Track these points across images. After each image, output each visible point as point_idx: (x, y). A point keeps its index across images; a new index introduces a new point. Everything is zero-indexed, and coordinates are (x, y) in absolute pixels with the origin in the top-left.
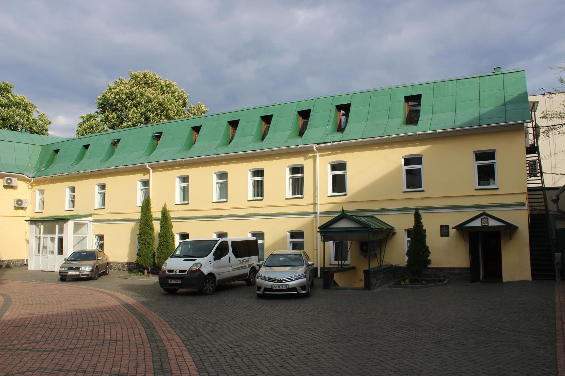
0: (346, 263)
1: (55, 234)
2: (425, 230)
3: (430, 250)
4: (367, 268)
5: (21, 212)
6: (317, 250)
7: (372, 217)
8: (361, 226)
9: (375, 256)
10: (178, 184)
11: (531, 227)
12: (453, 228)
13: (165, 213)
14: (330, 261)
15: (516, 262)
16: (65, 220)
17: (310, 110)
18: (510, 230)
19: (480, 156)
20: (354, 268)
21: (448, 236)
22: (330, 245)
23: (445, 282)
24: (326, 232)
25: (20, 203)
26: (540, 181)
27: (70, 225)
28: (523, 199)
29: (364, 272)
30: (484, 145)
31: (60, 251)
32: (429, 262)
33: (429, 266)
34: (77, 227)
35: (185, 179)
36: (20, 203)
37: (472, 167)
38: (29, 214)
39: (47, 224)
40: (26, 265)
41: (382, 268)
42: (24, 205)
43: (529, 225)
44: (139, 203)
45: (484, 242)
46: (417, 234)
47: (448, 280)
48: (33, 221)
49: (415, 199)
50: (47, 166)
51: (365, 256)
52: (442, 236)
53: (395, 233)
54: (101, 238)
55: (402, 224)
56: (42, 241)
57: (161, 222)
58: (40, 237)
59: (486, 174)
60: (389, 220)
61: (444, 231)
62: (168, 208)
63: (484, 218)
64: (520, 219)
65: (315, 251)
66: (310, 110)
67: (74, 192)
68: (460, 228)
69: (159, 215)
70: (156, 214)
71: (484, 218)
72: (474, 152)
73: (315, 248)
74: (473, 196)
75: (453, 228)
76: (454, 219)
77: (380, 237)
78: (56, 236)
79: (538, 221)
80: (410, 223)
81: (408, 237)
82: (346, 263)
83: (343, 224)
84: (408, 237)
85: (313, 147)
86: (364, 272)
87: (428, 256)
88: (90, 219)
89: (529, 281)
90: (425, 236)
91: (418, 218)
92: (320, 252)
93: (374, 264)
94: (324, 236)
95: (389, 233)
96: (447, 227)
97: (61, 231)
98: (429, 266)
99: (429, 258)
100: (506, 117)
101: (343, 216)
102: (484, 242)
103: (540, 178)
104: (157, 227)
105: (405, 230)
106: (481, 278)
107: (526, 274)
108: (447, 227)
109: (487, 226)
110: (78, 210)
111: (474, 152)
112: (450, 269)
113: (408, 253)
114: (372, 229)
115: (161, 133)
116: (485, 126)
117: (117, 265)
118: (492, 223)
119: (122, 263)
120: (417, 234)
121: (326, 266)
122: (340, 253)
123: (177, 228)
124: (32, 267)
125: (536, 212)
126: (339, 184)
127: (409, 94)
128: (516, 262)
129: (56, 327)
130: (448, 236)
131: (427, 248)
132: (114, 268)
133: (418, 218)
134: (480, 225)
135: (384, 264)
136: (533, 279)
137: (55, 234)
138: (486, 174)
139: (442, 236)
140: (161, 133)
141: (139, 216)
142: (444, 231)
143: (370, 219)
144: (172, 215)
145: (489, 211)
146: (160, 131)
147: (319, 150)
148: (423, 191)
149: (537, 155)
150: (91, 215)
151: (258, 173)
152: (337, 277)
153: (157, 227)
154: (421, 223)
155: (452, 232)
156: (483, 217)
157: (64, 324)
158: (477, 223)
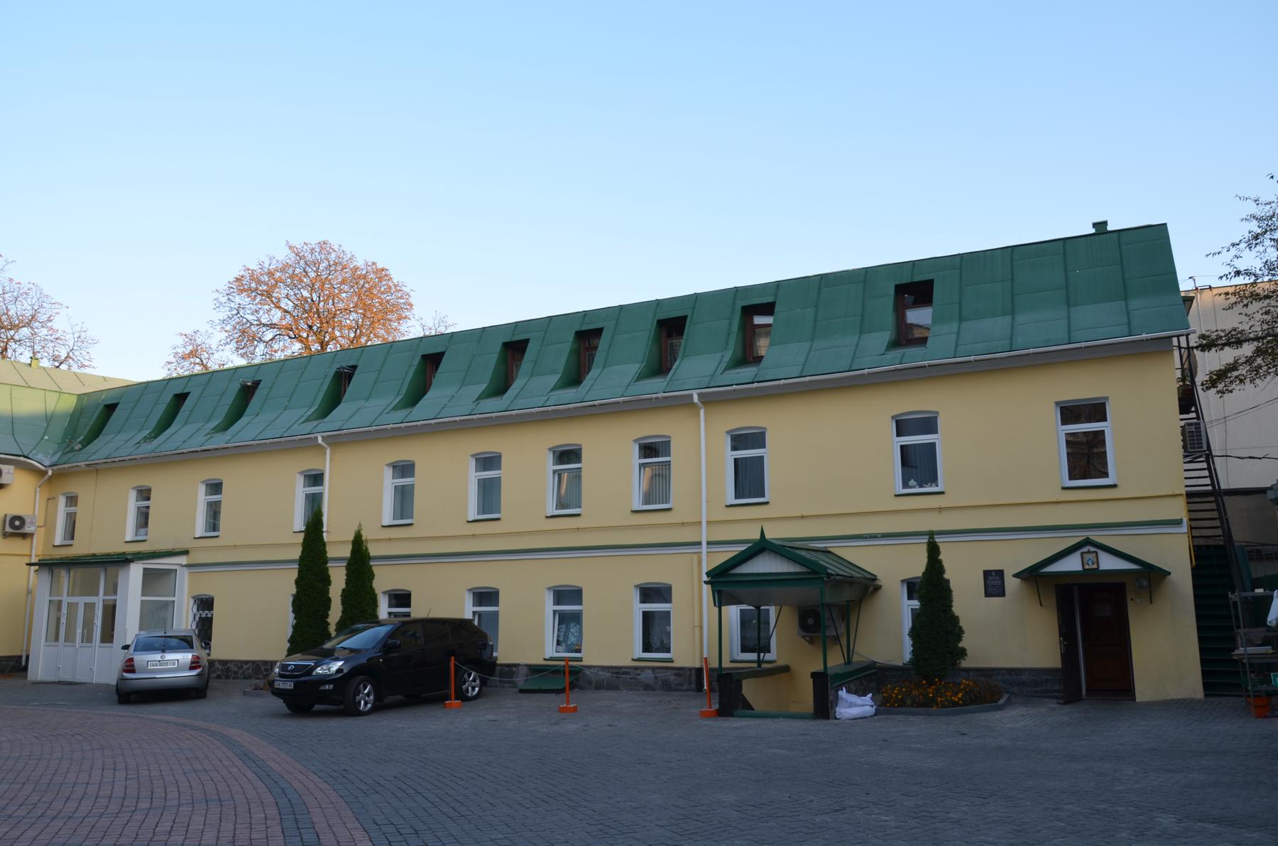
0: (768, 657)
1: (97, 594)
2: (948, 581)
3: (962, 624)
4: (819, 667)
5: (17, 546)
6: (701, 627)
7: (826, 552)
8: (804, 570)
9: (837, 639)
10: (389, 482)
11: (1197, 573)
12: (1016, 576)
13: (358, 543)
14: (731, 652)
15: (1165, 650)
16: (124, 560)
17: (685, 318)
18: (1150, 577)
19: (1070, 413)
20: (786, 669)
21: (1003, 594)
22: (733, 613)
23: (1001, 702)
24: (724, 582)
25: (17, 523)
26: (1206, 473)
27: (136, 572)
28: (1178, 510)
29: (814, 675)
30: (1080, 385)
31: (108, 636)
32: (963, 653)
33: (965, 664)
34: (151, 577)
35: (404, 469)
36: (17, 523)
37: (1053, 439)
38: (38, 549)
39: (78, 572)
40: (25, 669)
41: (850, 668)
42: (27, 529)
43: (1193, 569)
44: (299, 523)
45: (1093, 607)
46: (931, 589)
47: (1006, 696)
48: (48, 565)
49: (923, 514)
50: (87, 442)
51: (811, 642)
52: (987, 594)
53: (878, 588)
54: (205, 603)
55: (896, 566)
56: (64, 610)
57: (348, 568)
58: (60, 602)
59: (1087, 458)
60: (864, 558)
61: (993, 583)
62: (366, 535)
63: (1089, 552)
64: (1174, 554)
65: (697, 630)
66: (685, 318)
67: (148, 499)
68: (1033, 576)
69: (346, 552)
70: (338, 548)
71: (1089, 552)
72: (1057, 403)
73: (697, 623)
74: (1057, 503)
75: (1016, 576)
76: (1015, 557)
77: (847, 595)
78: (99, 601)
79: (1213, 564)
80: (917, 565)
81: (910, 598)
82: (768, 657)
83: (765, 565)
84: (910, 598)
85: (691, 396)
86: (814, 675)
87: (959, 639)
88: (183, 560)
89: (1200, 701)
90: (950, 591)
91: (933, 550)
92: (702, 631)
93: (836, 660)
94: (719, 592)
95: (867, 587)
96: (1000, 573)
97: (113, 588)
98: (965, 664)
99: (960, 645)
100: (1129, 324)
101: (761, 547)
102: (1093, 607)
103: (1205, 465)
104: (338, 579)
105: (903, 581)
106: (1084, 692)
107: (1190, 683)
108: (1000, 573)
109: (1096, 572)
110: (157, 538)
111: (1057, 403)
112: (1010, 671)
113: (914, 633)
114: (829, 575)
115: (354, 367)
116: (1083, 344)
117: (241, 667)
118: (1108, 563)
119: (253, 662)
120: (931, 589)
121: (724, 665)
122: (754, 637)
123: (384, 580)
124: (39, 670)
125: (1202, 542)
126: (749, 480)
127: (905, 280)
128: (1165, 650)
129: (49, 812)
130: (1003, 594)
131: (955, 620)
132: (236, 673)
133: (933, 550)
134: (1079, 568)
135: (855, 659)
136: (1206, 695)
137: (97, 594)
138: (1087, 458)
139: (987, 594)
140: (354, 367)
141: (296, 553)
142: (993, 583)
143: (821, 556)
144: (373, 550)
145: (1095, 536)
146: (351, 364)
147: (707, 400)
148: (942, 493)
149: (1193, 415)
150: (186, 552)
151: (568, 455)
152: (749, 689)
153: (338, 579)
154: (940, 562)
155: (1011, 584)
156: (1085, 549)
157: (72, 805)
158: (1072, 564)
